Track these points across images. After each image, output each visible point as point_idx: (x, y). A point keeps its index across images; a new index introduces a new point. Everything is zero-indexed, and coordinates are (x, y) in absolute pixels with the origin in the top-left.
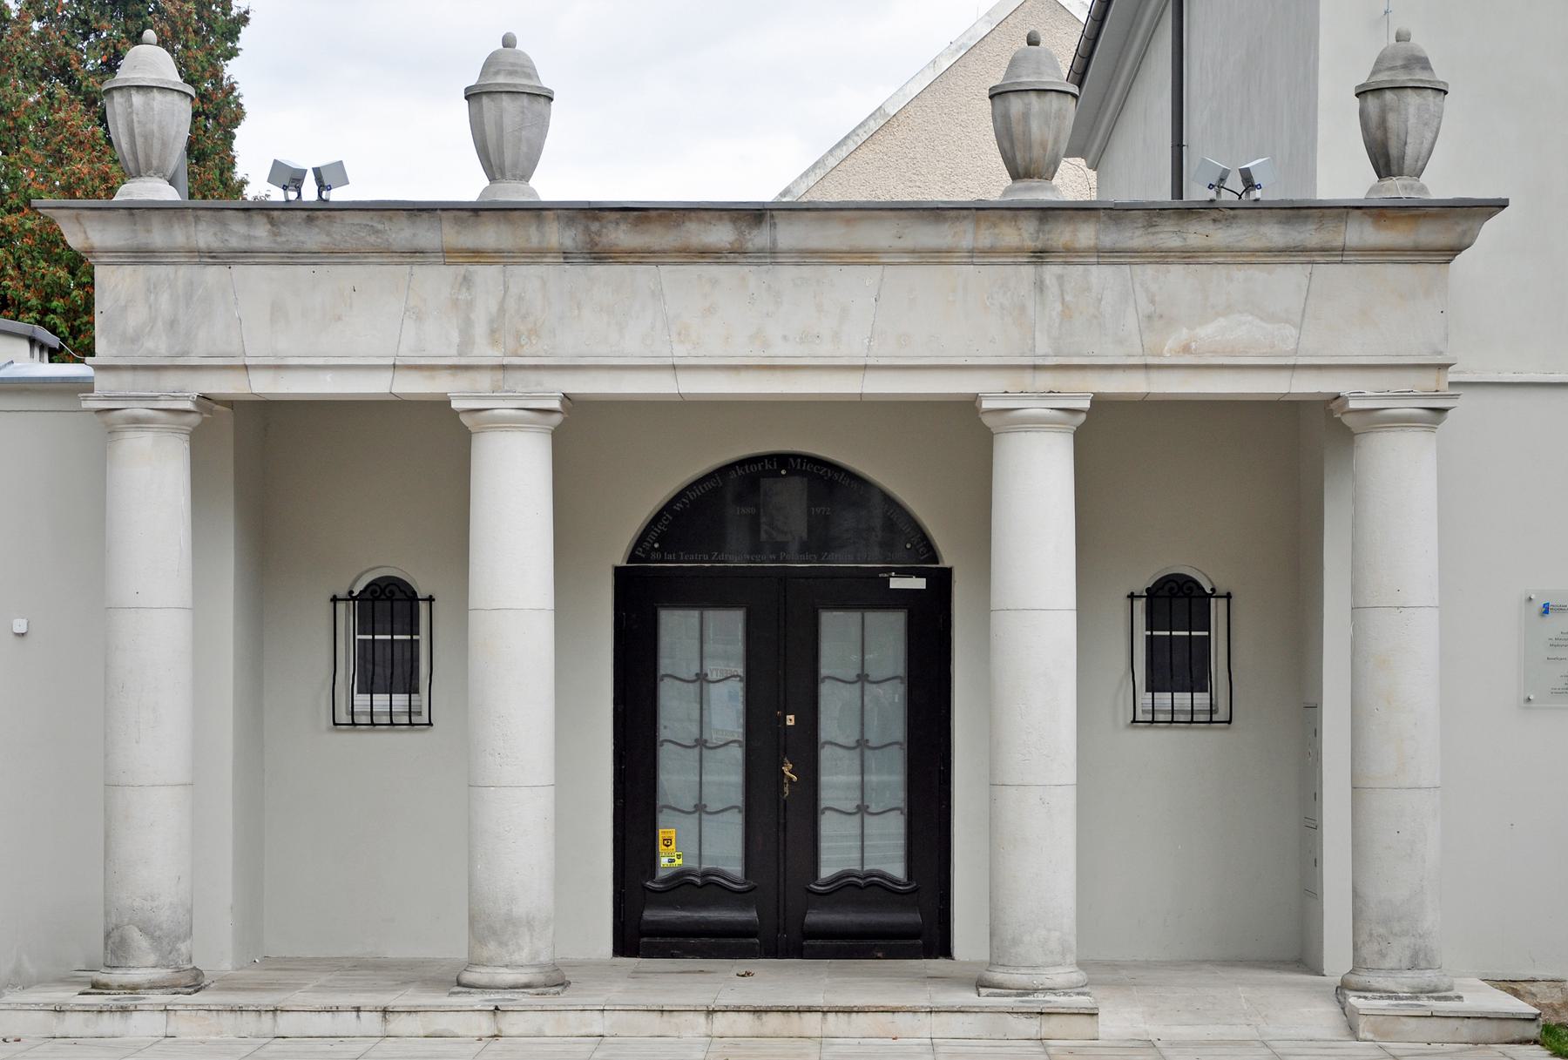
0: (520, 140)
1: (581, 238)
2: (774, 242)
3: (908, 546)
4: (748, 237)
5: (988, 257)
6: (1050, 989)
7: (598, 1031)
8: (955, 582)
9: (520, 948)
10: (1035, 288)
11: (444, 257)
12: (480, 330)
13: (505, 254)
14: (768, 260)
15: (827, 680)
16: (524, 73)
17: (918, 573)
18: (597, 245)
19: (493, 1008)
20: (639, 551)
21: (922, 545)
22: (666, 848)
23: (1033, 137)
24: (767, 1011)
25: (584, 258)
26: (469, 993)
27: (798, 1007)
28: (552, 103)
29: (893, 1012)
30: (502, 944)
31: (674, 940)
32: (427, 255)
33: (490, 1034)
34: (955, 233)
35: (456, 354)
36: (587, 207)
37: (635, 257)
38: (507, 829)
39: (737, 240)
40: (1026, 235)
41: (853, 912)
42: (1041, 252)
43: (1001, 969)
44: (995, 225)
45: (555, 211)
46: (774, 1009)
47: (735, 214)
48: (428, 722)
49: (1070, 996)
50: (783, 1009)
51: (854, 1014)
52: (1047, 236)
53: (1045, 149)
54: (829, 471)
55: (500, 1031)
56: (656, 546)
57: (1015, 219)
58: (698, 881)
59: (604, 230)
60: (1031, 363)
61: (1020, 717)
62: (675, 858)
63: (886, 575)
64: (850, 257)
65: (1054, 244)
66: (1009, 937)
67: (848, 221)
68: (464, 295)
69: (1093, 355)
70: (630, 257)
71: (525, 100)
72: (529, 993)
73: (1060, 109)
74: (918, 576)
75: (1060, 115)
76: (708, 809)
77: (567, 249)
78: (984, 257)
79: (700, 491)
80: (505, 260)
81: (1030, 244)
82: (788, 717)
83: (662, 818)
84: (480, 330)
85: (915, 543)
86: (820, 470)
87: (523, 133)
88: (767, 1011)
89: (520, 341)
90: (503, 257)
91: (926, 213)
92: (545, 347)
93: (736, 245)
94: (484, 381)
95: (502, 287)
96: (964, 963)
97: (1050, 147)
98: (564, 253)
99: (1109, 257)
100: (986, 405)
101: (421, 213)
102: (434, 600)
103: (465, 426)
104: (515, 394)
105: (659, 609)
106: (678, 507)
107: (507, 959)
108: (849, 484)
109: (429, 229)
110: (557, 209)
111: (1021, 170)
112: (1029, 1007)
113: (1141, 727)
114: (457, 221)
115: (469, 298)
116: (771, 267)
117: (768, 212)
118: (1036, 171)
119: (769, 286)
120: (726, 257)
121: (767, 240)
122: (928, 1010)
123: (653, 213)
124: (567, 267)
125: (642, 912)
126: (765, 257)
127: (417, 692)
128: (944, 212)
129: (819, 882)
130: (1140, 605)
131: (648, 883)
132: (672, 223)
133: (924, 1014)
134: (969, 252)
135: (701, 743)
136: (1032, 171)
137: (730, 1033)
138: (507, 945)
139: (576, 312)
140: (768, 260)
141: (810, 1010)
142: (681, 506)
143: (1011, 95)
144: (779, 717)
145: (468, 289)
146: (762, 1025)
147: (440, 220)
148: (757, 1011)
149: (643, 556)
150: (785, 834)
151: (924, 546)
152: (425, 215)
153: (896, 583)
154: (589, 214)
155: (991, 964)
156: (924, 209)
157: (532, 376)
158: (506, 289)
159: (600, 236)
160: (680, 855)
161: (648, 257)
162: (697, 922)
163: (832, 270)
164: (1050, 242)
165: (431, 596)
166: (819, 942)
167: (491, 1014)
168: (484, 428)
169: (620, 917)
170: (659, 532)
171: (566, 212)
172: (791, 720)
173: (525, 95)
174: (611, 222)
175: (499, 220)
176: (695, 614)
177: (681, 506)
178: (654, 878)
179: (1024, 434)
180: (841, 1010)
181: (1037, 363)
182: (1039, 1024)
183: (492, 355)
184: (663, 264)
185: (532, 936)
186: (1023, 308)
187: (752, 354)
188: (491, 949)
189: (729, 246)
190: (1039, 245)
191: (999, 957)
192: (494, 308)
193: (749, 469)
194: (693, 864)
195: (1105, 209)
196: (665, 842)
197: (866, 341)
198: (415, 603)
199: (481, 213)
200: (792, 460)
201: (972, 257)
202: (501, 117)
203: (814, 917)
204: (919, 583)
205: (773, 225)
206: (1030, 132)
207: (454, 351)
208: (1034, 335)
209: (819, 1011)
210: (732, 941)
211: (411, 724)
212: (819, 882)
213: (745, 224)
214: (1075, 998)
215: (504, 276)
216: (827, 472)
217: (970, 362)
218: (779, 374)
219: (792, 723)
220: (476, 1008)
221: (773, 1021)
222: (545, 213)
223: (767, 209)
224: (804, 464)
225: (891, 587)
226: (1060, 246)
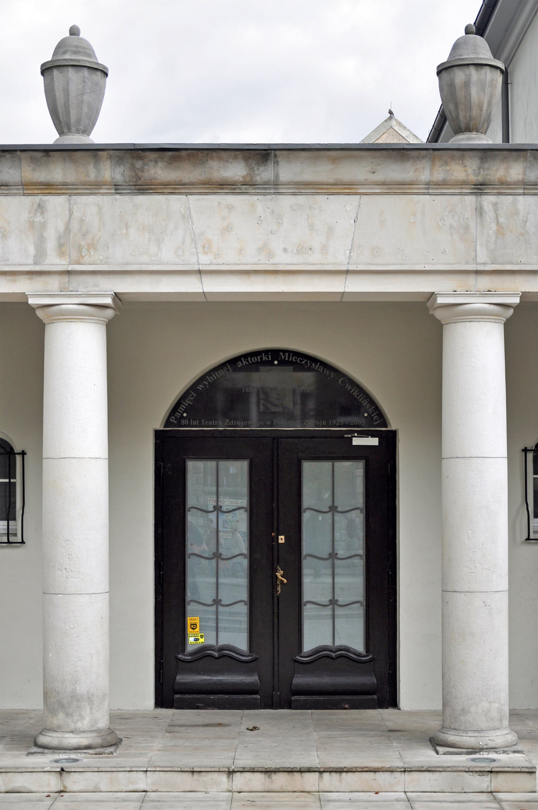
0: (82, 102)
1: (128, 173)
2: (277, 176)
3: (366, 415)
4: (257, 172)
5: (440, 188)
6: (492, 748)
7: (142, 787)
8: (399, 440)
9: (82, 717)
10: (476, 213)
11: (23, 189)
12: (51, 245)
13: (70, 187)
14: (272, 191)
15: (307, 511)
16: (85, 53)
17: (373, 434)
18: (140, 178)
19: (59, 770)
20: (173, 419)
21: (375, 414)
22: (192, 630)
23: (472, 100)
24: (276, 771)
25: (130, 189)
26: (43, 753)
27: (300, 768)
28: (108, 79)
29: (375, 772)
30: (68, 715)
31: (199, 696)
32: (10, 187)
33: (57, 790)
34: (416, 169)
35: (33, 264)
36: (133, 148)
37: (169, 189)
38: (72, 627)
39: (248, 174)
40: (470, 171)
41: (327, 676)
42: (481, 185)
43: (453, 732)
44: (446, 163)
45: (108, 152)
46: (281, 770)
47: (246, 153)
48: (21, 541)
49: (508, 754)
50: (288, 770)
51: (344, 774)
52: (486, 172)
53: (481, 109)
54: (309, 362)
55: (65, 787)
56: (185, 415)
57: (462, 158)
58: (216, 654)
59: (146, 167)
60: (475, 269)
61: (467, 540)
62: (199, 638)
63: (350, 436)
64: (335, 189)
65: (492, 178)
66: (460, 708)
67: (334, 160)
68: (38, 219)
69: (521, 263)
70: (165, 188)
71: (86, 72)
72: (89, 753)
73: (492, 80)
74: (373, 436)
75: (492, 84)
76: (223, 603)
77: (118, 182)
78: (437, 189)
79: (196, 423)
80: (70, 192)
81: (473, 178)
82: (280, 537)
83: (190, 608)
84: (51, 245)
85: (370, 413)
86: (302, 361)
87: (84, 97)
88: (276, 771)
89: (81, 253)
90: (69, 189)
91: (394, 153)
92: (101, 258)
93: (248, 179)
94: (54, 283)
95: (67, 212)
96: (410, 713)
97: (485, 108)
98: (115, 185)
99: (532, 189)
100: (440, 300)
101: (4, 154)
102: (26, 454)
103: (41, 320)
104: (77, 293)
105: (187, 460)
106: (200, 387)
107: (72, 726)
108: (323, 371)
109: (11, 167)
110: (110, 150)
111: (463, 126)
112: (481, 767)
113: (533, 543)
114: (32, 159)
115: (43, 220)
116: (274, 196)
117: (273, 152)
118: (475, 127)
119: (273, 211)
120: (240, 189)
121: (271, 174)
122: (403, 770)
123: (184, 153)
124: (118, 196)
125: (176, 677)
126: (270, 189)
127: (14, 519)
128: (408, 152)
129: (302, 654)
130: (530, 456)
131: (180, 656)
132: (199, 162)
133: (399, 773)
134: (426, 185)
135: (217, 556)
136: (471, 127)
137: (246, 789)
138: (72, 716)
139: (125, 231)
140: (272, 191)
141: (309, 770)
142: (203, 387)
143: (455, 68)
144: (273, 537)
145: (42, 214)
146: (272, 782)
147: (20, 159)
148: (268, 772)
149: (175, 422)
150: (278, 620)
151: (377, 415)
152: (8, 155)
153: (357, 441)
154: (135, 154)
155: (443, 727)
156: (393, 150)
157: (90, 280)
158: (71, 213)
159: (143, 171)
160: (202, 636)
161: (180, 188)
162: (216, 683)
163: (320, 199)
164: (488, 177)
165: (23, 451)
166: (303, 698)
167: (58, 775)
168: (54, 320)
169: (160, 680)
170: (187, 405)
171: (117, 153)
172: (282, 539)
173: (86, 69)
174: (151, 161)
175: (65, 160)
176: (211, 464)
177: (203, 387)
178: (184, 652)
179: (469, 323)
180: (334, 770)
181: (478, 269)
182: (489, 780)
183: (61, 264)
184: (192, 194)
185: (91, 709)
186: (467, 228)
187: (260, 262)
188: (60, 719)
189: (241, 179)
190: (480, 179)
191: (451, 722)
192: (61, 227)
193: (251, 360)
194: (213, 642)
195: (532, 150)
196: (192, 626)
197: (348, 252)
198: (12, 456)
199: (51, 153)
200: (281, 353)
201: (428, 189)
202: (68, 84)
203: (300, 680)
204: (374, 441)
205: (277, 163)
206: (470, 96)
207: (31, 261)
208: (476, 247)
209: (317, 771)
210: (240, 697)
211: (9, 542)
212: (302, 654)
213: (254, 162)
214: (512, 755)
215: (69, 204)
216: (307, 362)
217: (428, 268)
218: (280, 278)
219: (283, 541)
220: (46, 769)
221: (280, 780)
222: (100, 153)
223: (271, 150)
224: (291, 356)
225: (353, 444)
226: (496, 180)
